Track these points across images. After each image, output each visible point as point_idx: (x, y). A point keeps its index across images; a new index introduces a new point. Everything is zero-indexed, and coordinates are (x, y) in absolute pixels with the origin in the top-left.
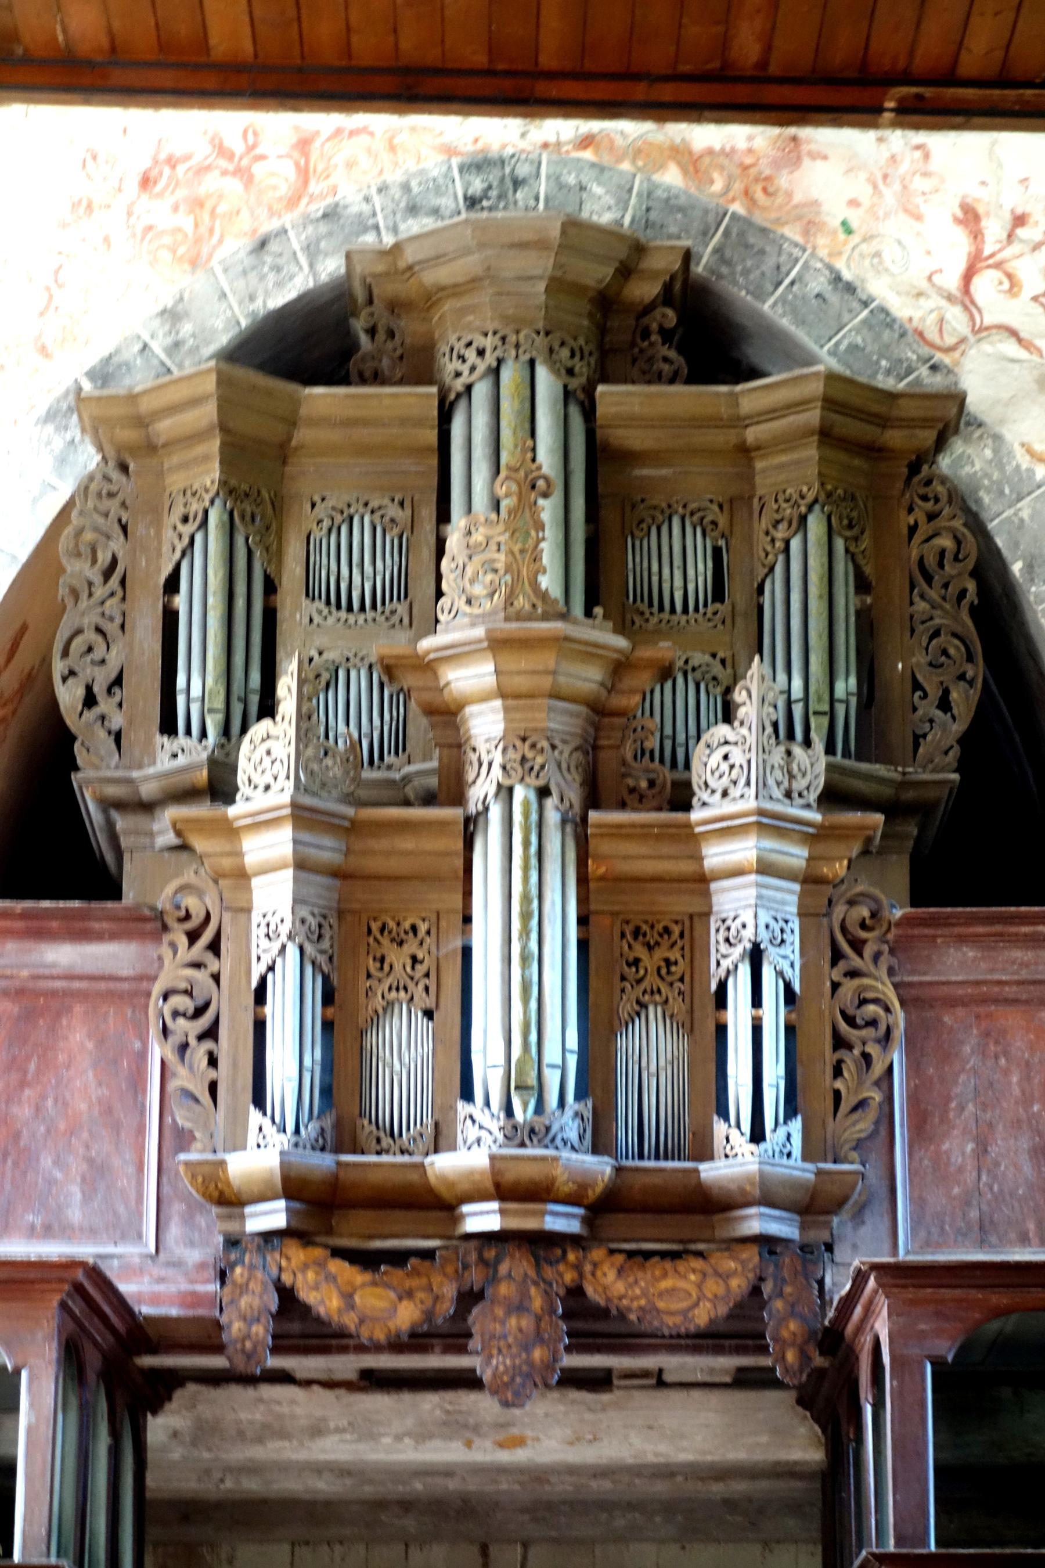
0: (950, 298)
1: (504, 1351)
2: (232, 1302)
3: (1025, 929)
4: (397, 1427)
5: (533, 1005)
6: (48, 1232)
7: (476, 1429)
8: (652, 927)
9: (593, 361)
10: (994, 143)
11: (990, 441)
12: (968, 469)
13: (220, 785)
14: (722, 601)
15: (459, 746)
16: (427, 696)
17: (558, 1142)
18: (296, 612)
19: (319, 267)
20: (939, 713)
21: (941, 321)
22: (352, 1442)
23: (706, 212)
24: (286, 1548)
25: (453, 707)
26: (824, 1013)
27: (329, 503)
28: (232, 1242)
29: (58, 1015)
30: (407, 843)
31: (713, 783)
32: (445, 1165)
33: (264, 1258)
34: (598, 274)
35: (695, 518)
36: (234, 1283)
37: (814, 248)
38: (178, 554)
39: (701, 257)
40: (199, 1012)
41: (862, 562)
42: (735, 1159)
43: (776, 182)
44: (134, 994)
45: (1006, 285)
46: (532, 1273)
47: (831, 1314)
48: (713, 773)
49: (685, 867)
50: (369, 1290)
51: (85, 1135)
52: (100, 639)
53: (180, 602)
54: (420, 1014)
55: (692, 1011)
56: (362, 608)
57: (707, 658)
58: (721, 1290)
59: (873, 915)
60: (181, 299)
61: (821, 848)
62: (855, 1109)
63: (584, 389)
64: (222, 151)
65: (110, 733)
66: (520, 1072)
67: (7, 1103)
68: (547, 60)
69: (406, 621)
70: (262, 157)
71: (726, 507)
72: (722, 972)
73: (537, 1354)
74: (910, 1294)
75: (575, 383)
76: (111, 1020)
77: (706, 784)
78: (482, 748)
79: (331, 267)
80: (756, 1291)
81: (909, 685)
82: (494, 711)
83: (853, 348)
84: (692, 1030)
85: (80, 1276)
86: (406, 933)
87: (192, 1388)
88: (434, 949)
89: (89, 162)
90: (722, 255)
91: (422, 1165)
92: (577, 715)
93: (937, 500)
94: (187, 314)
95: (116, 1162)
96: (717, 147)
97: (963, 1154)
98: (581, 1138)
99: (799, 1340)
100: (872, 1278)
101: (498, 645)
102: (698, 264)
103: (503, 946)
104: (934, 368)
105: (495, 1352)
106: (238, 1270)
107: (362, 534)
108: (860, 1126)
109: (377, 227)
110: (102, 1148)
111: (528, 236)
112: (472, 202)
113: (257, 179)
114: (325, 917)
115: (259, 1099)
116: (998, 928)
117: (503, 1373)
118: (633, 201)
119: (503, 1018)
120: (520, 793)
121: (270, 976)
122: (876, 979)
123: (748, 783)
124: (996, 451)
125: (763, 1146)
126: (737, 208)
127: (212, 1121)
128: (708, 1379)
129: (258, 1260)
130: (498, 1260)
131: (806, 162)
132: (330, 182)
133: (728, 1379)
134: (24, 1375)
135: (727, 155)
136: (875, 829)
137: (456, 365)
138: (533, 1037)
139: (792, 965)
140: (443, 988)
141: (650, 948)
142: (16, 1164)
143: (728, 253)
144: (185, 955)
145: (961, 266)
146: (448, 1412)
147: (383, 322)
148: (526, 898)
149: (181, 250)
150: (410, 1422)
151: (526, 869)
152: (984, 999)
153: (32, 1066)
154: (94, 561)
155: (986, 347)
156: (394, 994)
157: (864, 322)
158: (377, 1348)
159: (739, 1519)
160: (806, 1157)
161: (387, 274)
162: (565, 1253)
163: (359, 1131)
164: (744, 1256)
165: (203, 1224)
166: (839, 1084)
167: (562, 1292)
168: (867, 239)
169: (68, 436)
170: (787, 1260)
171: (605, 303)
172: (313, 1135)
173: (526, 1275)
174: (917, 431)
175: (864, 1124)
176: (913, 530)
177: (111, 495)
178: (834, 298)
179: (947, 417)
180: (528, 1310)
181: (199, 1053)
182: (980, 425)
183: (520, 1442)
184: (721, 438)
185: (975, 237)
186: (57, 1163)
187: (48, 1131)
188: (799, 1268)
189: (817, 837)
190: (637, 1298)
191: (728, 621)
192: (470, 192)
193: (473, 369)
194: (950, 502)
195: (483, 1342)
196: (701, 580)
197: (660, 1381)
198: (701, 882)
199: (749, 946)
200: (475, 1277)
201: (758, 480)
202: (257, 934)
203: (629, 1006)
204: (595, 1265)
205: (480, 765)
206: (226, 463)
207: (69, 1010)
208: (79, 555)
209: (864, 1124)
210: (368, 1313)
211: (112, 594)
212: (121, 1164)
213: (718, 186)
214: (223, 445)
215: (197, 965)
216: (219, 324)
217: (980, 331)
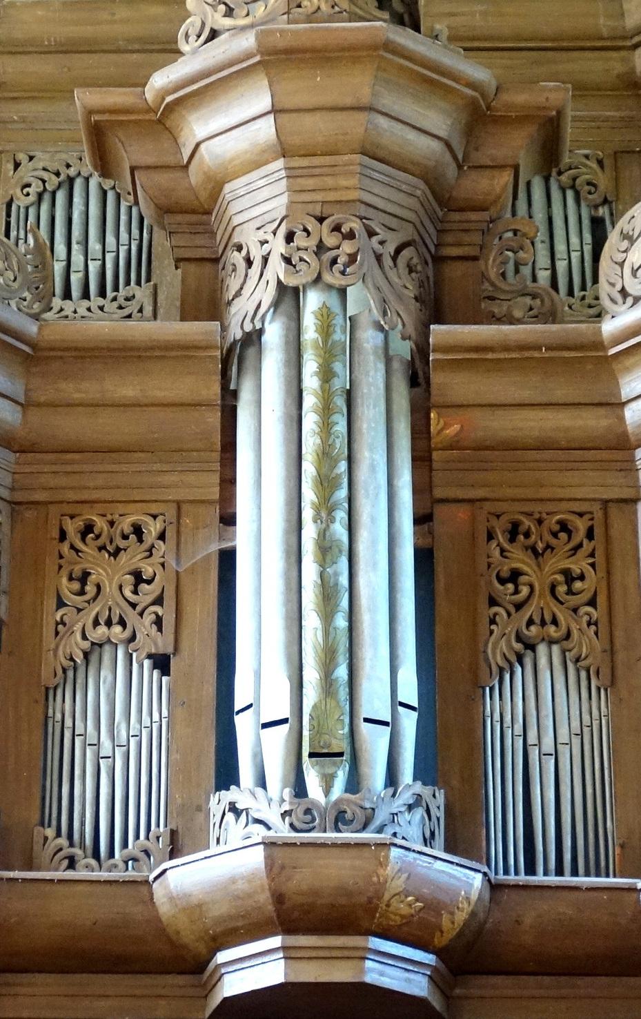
5: (341, 622)
8: (540, 522)
30: (126, 387)
32: (187, 879)
54: (147, 663)
56: (86, 295)
66: (317, 731)
69: (148, 310)
71: (606, 162)
78: (249, 238)
84: (613, 682)
103: (287, 532)
138: (342, 672)
148: (325, 455)
156: (102, 629)
163: (37, 847)
203: (503, 643)
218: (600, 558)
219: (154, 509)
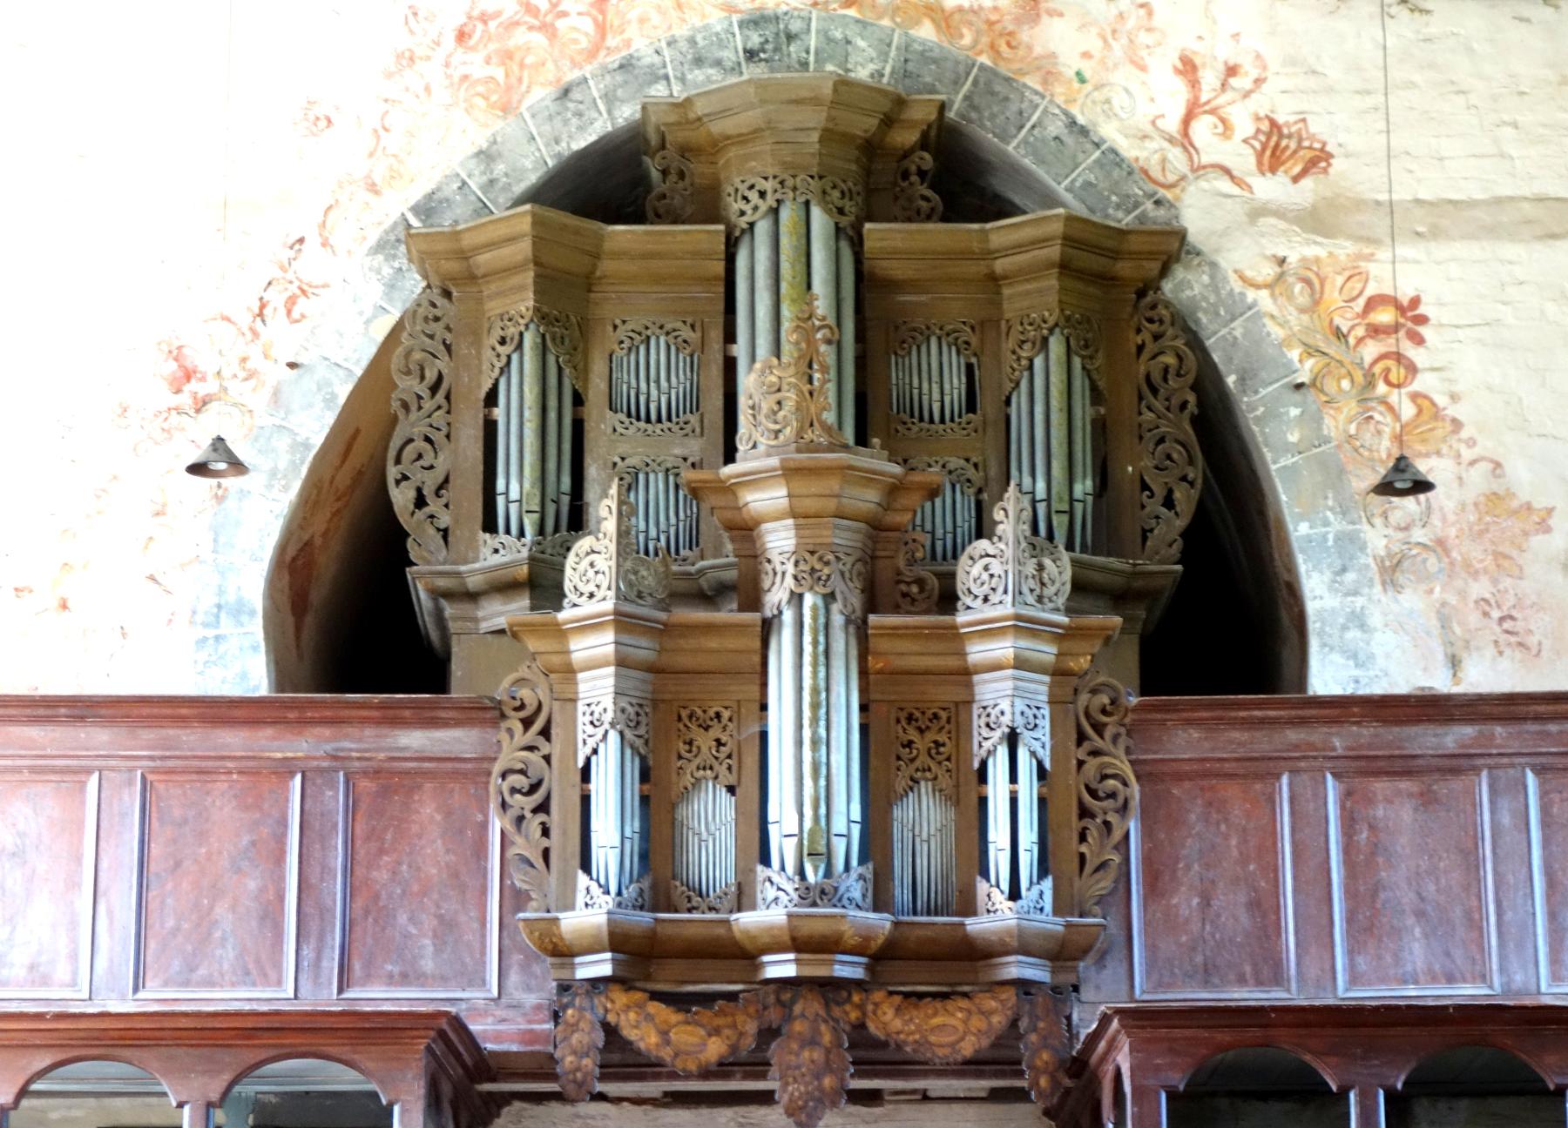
0: (1171, 140)
2: (565, 1039)
5: (822, 782)
6: (404, 979)
9: (859, 199)
11: (1206, 268)
12: (1188, 293)
13: (543, 584)
14: (974, 412)
15: (756, 557)
16: (728, 514)
17: (845, 902)
18: (602, 424)
19: (617, 113)
20: (1164, 510)
21: (1164, 160)
23: (957, 63)
25: (750, 523)
26: (1071, 787)
27: (629, 326)
28: (564, 988)
30: (713, 643)
31: (975, 590)
32: (746, 920)
34: (866, 125)
35: (950, 339)
36: (567, 1023)
38: (497, 371)
40: (534, 788)
41: (1095, 376)
42: (996, 915)
44: (477, 773)
45: (1221, 129)
46: (822, 1012)
47: (1079, 1046)
49: (952, 662)
50: (683, 1028)
51: (435, 896)
52: (428, 446)
53: (499, 413)
55: (957, 786)
56: (659, 420)
57: (962, 462)
58: (983, 1026)
59: (1113, 702)
60: (495, 142)
61: (1067, 645)
62: (1097, 870)
63: (853, 226)
66: (811, 842)
69: (698, 430)
70: (564, 14)
72: (983, 753)
74: (1147, 1033)
75: (845, 221)
76: (457, 797)
77: (969, 591)
78: (776, 559)
79: (627, 113)
80: (1014, 1023)
81: (1138, 484)
82: (786, 528)
83: (1088, 185)
87: (517, 1105)
91: (727, 922)
92: (857, 531)
93: (1161, 322)
94: (500, 155)
95: (462, 918)
96: (966, 5)
97: (1190, 906)
98: (864, 896)
99: (1051, 1068)
101: (790, 472)
104: (1158, 203)
106: (570, 1012)
107: (658, 351)
108: (1102, 885)
109: (667, 78)
111: (805, 94)
112: (751, 55)
114: (641, 706)
115: (586, 866)
118: (893, 53)
120: (809, 600)
121: (594, 759)
122: (1115, 757)
123: (1005, 592)
124: (1212, 277)
125: (1020, 902)
126: (984, 59)
128: (968, 1094)
129: (586, 1004)
130: (793, 1002)
131: (1045, 18)
132: (625, 36)
133: (983, 1094)
134: (396, 1109)
135: (974, 12)
137: (741, 205)
138: (823, 810)
141: (921, 731)
142: (376, 921)
143: (976, 100)
144: (521, 738)
145: (1181, 111)
147: (675, 164)
148: (815, 691)
149: (494, 98)
151: (815, 665)
153: (389, 837)
154: (422, 378)
155: (1203, 184)
157: (1096, 161)
158: (688, 1076)
160: (1057, 911)
161: (679, 124)
162: (850, 995)
164: (1004, 996)
166: (1084, 849)
168: (1097, 88)
169: (396, 265)
171: (871, 149)
172: (634, 895)
174: (1144, 263)
175: (1105, 883)
176: (1140, 348)
177: (437, 319)
178: (1069, 140)
179: (1170, 248)
180: (818, 1044)
181: (534, 824)
182: (1198, 254)
186: (410, 919)
187: (404, 892)
189: (1064, 636)
190: (912, 1033)
191: (980, 430)
192: (749, 46)
193: (756, 208)
194: (1173, 324)
197: (925, 1097)
198: (966, 674)
199: (1007, 730)
200: (774, 1016)
201: (1006, 306)
202: (582, 720)
205: (775, 574)
206: (539, 293)
207: (420, 787)
208: (408, 373)
209: (1105, 883)
213: (967, 40)
214: (537, 276)
215: (531, 748)
216: (528, 164)
217: (1198, 169)
218: (953, 735)
219: (727, 704)
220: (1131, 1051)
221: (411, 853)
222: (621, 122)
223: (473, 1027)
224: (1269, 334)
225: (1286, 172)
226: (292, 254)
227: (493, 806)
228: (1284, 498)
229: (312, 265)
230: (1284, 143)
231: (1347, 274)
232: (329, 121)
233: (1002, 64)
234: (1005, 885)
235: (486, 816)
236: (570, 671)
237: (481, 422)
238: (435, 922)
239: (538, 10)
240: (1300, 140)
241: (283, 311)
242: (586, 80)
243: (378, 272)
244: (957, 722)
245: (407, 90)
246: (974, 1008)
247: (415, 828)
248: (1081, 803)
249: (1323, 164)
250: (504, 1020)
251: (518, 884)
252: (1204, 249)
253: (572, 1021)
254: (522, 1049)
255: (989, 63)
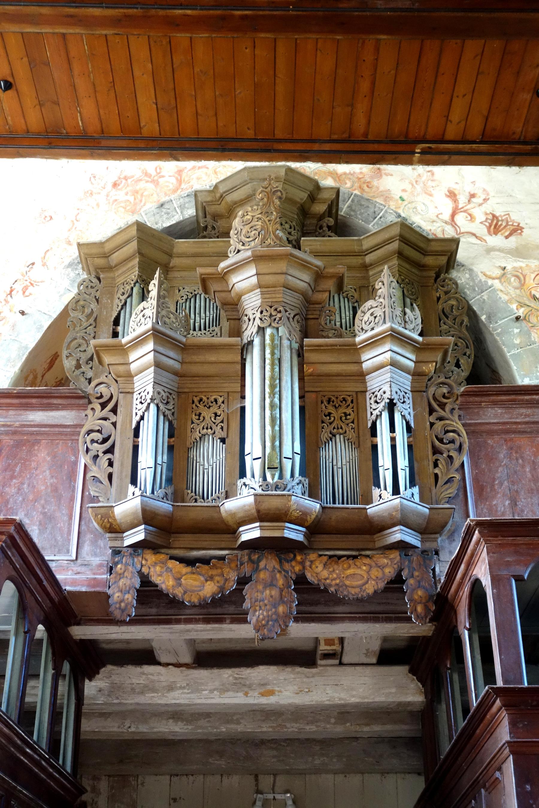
0: (446, 223)
1: (263, 608)
3: (527, 397)
4: (211, 686)
5: (277, 428)
7: (250, 687)
8: (337, 398)
10: (459, 170)
11: (467, 271)
19: (185, 213)
20: (456, 369)
22: (188, 693)
24: (168, 777)
28: (116, 552)
29: (33, 445)
30: (212, 357)
33: (133, 560)
36: (116, 573)
37: (389, 206)
38: (120, 307)
39: (343, 209)
40: (105, 440)
43: (372, 183)
45: (469, 218)
46: (277, 566)
48: (365, 323)
49: (353, 368)
50: (189, 576)
51: (43, 502)
54: (218, 440)
56: (200, 330)
58: (380, 575)
62: (446, 483)
64: (146, 174)
65: (86, 379)
66: (270, 461)
67: (3, 487)
68: (279, 134)
69: (219, 334)
70: (163, 176)
72: (374, 417)
73: (281, 609)
74: (499, 540)
76: (60, 447)
77: (362, 329)
78: (249, 312)
85: (12, 529)
86: (212, 403)
88: (226, 410)
89: (92, 179)
90: (351, 208)
95: (58, 514)
96: (348, 172)
97: (504, 506)
99: (424, 601)
100: (477, 532)
102: (341, 212)
103: (261, 401)
105: (258, 608)
106: (119, 566)
110: (51, 508)
113: (160, 184)
114: (171, 394)
115: (134, 481)
116: (513, 397)
117: (263, 620)
119: (261, 385)
122: (453, 421)
126: (357, 192)
127: (109, 492)
129: (130, 561)
130: (259, 560)
131: (384, 177)
132: (190, 184)
136: (449, 345)
138: (277, 443)
139: (409, 414)
140: (230, 427)
143: (354, 208)
144: (99, 413)
145: (450, 212)
146: (236, 679)
148: (272, 378)
149: (128, 208)
150: (217, 684)
152: (507, 431)
153: (18, 469)
154: (83, 312)
156: (205, 430)
159: (371, 759)
162: (295, 556)
163: (185, 496)
164: (392, 556)
165: (102, 545)
166: (437, 471)
167: (294, 577)
169: (77, 272)
170: (415, 558)
173: (274, 568)
175: (452, 490)
176: (439, 299)
180: (275, 586)
181: (104, 460)
182: (463, 266)
183: (272, 693)
184: (355, 261)
185: (455, 202)
186: (26, 515)
187: (24, 499)
188: (422, 563)
190: (335, 579)
195: (251, 602)
196: (348, 318)
199: (388, 401)
200: (247, 569)
203: (326, 434)
204: (312, 562)
209: (452, 490)
210: (189, 587)
211: (91, 325)
212: (61, 516)
213: (349, 185)
215: (105, 419)
218: (355, 409)
219: (221, 394)
220: (488, 553)
221: (30, 478)
222: (187, 216)
223: (59, 577)
224: (500, 298)
225: (502, 234)
226: (28, 269)
227: (82, 449)
228: (515, 368)
229: (35, 274)
230: (500, 223)
231: (536, 273)
232: (51, 218)
233: (365, 194)
234: (390, 488)
235: (77, 458)
236: (129, 376)
237: (111, 331)
238: (41, 516)
239: (151, 175)
240: (507, 222)
241: (22, 292)
242: (172, 201)
243: (68, 275)
244: (357, 403)
245: (89, 205)
246: (373, 564)
247: (33, 465)
248: (433, 447)
249: (519, 231)
250: (79, 573)
251: (92, 493)
252: (466, 264)
253: (120, 572)
254: (88, 590)
255: (359, 193)
